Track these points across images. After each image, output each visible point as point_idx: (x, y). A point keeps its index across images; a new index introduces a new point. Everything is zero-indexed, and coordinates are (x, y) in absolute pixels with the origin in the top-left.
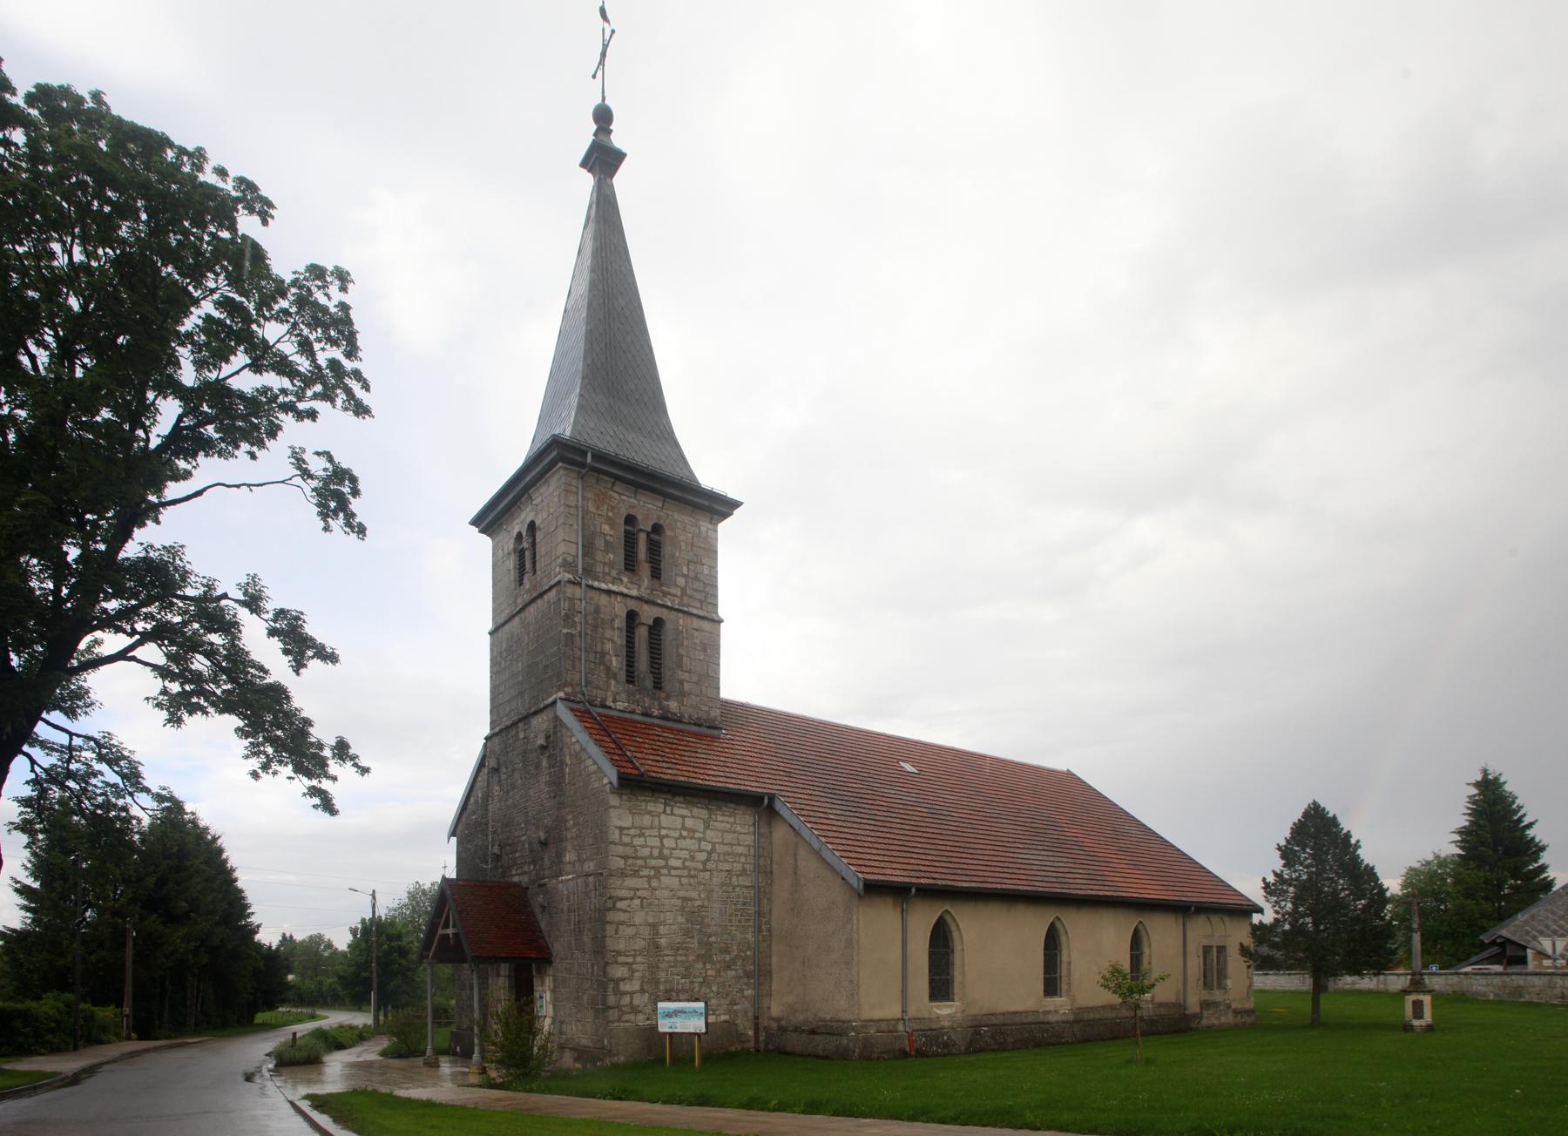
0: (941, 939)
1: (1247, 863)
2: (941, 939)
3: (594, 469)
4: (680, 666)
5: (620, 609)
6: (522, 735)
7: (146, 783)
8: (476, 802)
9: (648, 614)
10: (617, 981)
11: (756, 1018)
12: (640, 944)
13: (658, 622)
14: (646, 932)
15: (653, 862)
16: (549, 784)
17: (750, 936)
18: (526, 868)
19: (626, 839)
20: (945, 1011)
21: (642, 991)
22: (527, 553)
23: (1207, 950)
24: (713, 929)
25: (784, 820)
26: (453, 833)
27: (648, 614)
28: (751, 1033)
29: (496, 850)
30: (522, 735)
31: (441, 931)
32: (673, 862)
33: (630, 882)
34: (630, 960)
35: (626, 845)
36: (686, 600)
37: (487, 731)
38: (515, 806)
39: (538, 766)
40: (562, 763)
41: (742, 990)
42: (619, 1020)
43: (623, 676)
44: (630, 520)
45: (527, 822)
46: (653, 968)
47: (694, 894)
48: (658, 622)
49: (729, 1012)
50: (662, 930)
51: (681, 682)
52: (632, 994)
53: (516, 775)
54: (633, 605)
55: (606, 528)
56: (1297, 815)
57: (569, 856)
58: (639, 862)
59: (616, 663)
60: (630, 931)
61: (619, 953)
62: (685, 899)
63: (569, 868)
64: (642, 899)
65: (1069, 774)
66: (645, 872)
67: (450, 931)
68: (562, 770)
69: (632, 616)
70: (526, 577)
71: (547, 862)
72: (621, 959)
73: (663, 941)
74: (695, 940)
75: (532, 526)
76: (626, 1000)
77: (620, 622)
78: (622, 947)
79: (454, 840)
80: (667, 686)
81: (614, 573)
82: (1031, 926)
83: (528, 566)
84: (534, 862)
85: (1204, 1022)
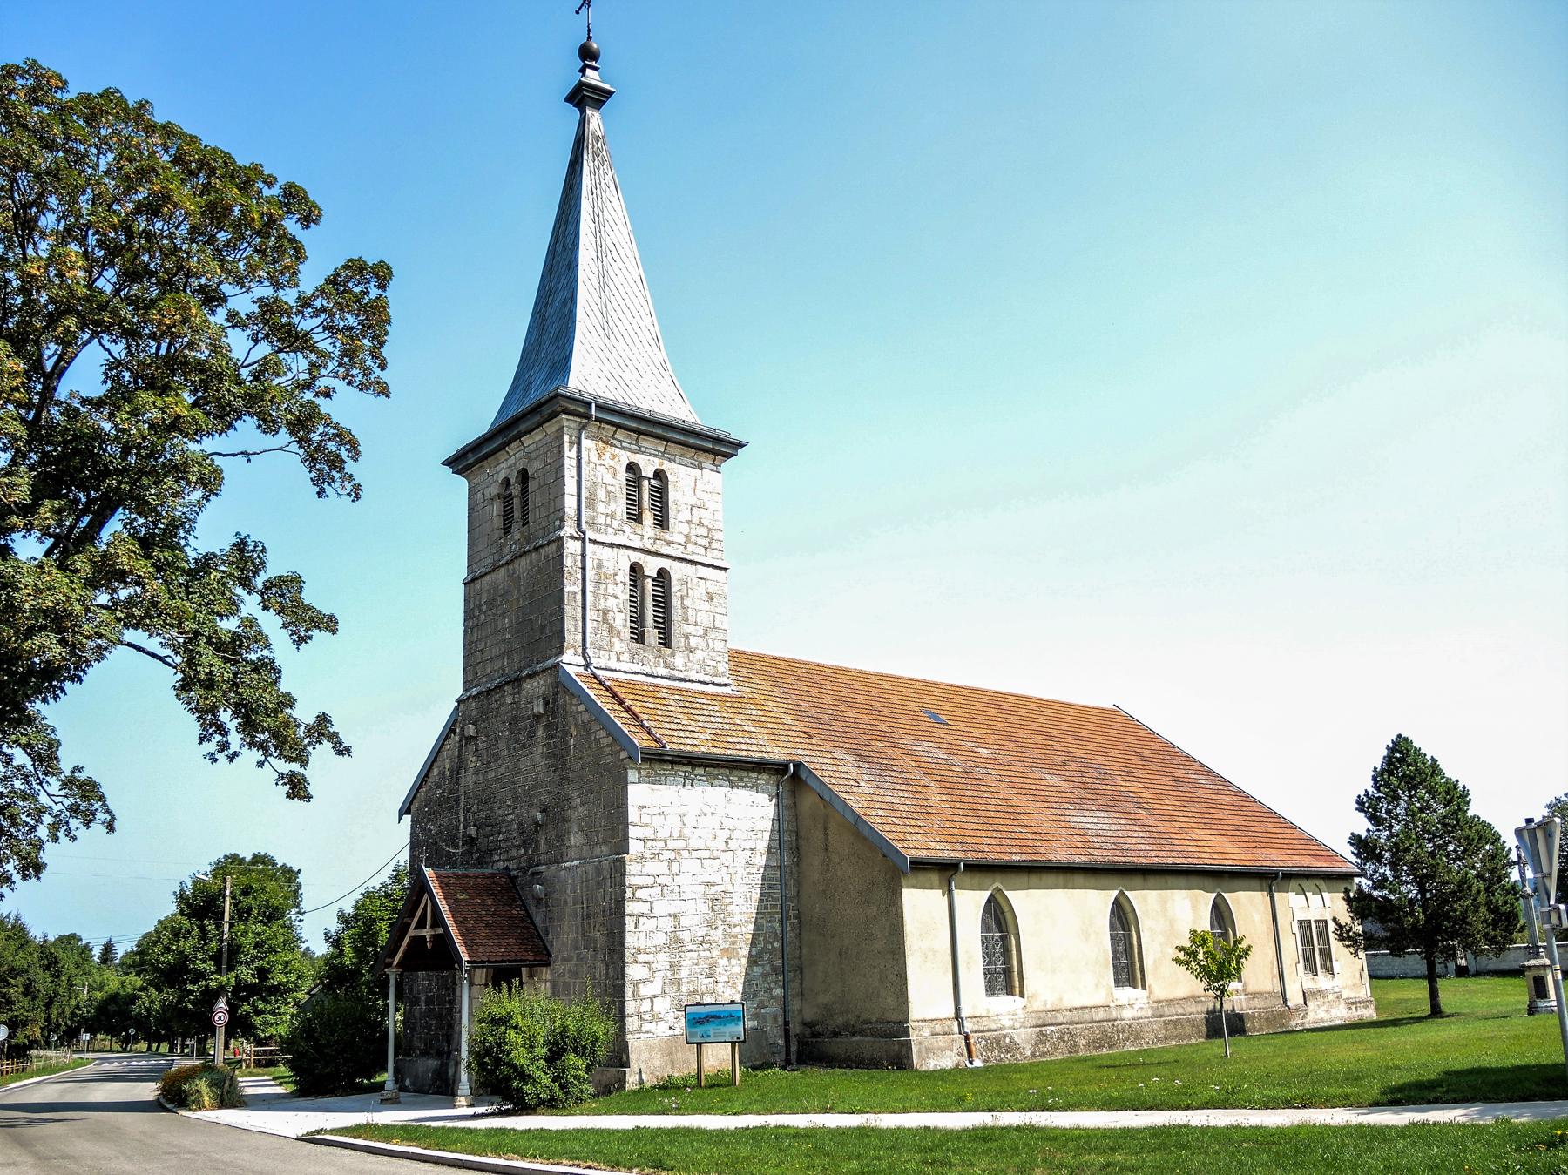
0: (998, 919)
1: (1328, 810)
2: (998, 919)
3: (597, 419)
4: (686, 620)
5: (625, 560)
6: (509, 700)
7: (1204, 925)
8: (442, 773)
9: (651, 566)
10: (636, 984)
11: (786, 1023)
12: (661, 939)
13: (663, 574)
14: (666, 924)
15: (672, 844)
16: (547, 756)
17: (777, 925)
18: (514, 853)
19: (645, 819)
20: (1004, 1012)
21: (664, 994)
22: (516, 501)
23: (1305, 927)
24: (736, 919)
25: (811, 788)
26: (405, 810)
27: (651, 566)
28: (781, 1042)
29: (472, 832)
30: (509, 700)
31: (411, 933)
32: (694, 843)
33: (651, 868)
34: (650, 958)
35: (646, 825)
36: (690, 547)
37: (458, 692)
38: (497, 780)
39: (532, 735)
40: (566, 733)
41: (770, 989)
42: (639, 1030)
43: (626, 634)
44: (632, 468)
45: (515, 799)
46: (675, 966)
47: (715, 878)
48: (663, 574)
49: (756, 1016)
50: (684, 921)
51: (687, 637)
52: (652, 998)
53: (501, 744)
54: (637, 557)
55: (608, 479)
56: (1377, 759)
57: (575, 839)
58: (661, 844)
59: (621, 621)
60: (651, 924)
61: (639, 951)
62: (709, 884)
63: (573, 853)
64: (663, 886)
65: (1117, 711)
66: (667, 855)
67: (427, 932)
68: (565, 742)
69: (635, 569)
70: (515, 527)
71: (543, 847)
72: (641, 958)
73: (686, 936)
74: (720, 932)
75: (524, 476)
76: (646, 1006)
77: (624, 575)
78: (642, 944)
79: (407, 819)
80: (678, 641)
81: (616, 524)
82: (1097, 902)
83: (517, 514)
84: (525, 845)
85: (1311, 1017)
